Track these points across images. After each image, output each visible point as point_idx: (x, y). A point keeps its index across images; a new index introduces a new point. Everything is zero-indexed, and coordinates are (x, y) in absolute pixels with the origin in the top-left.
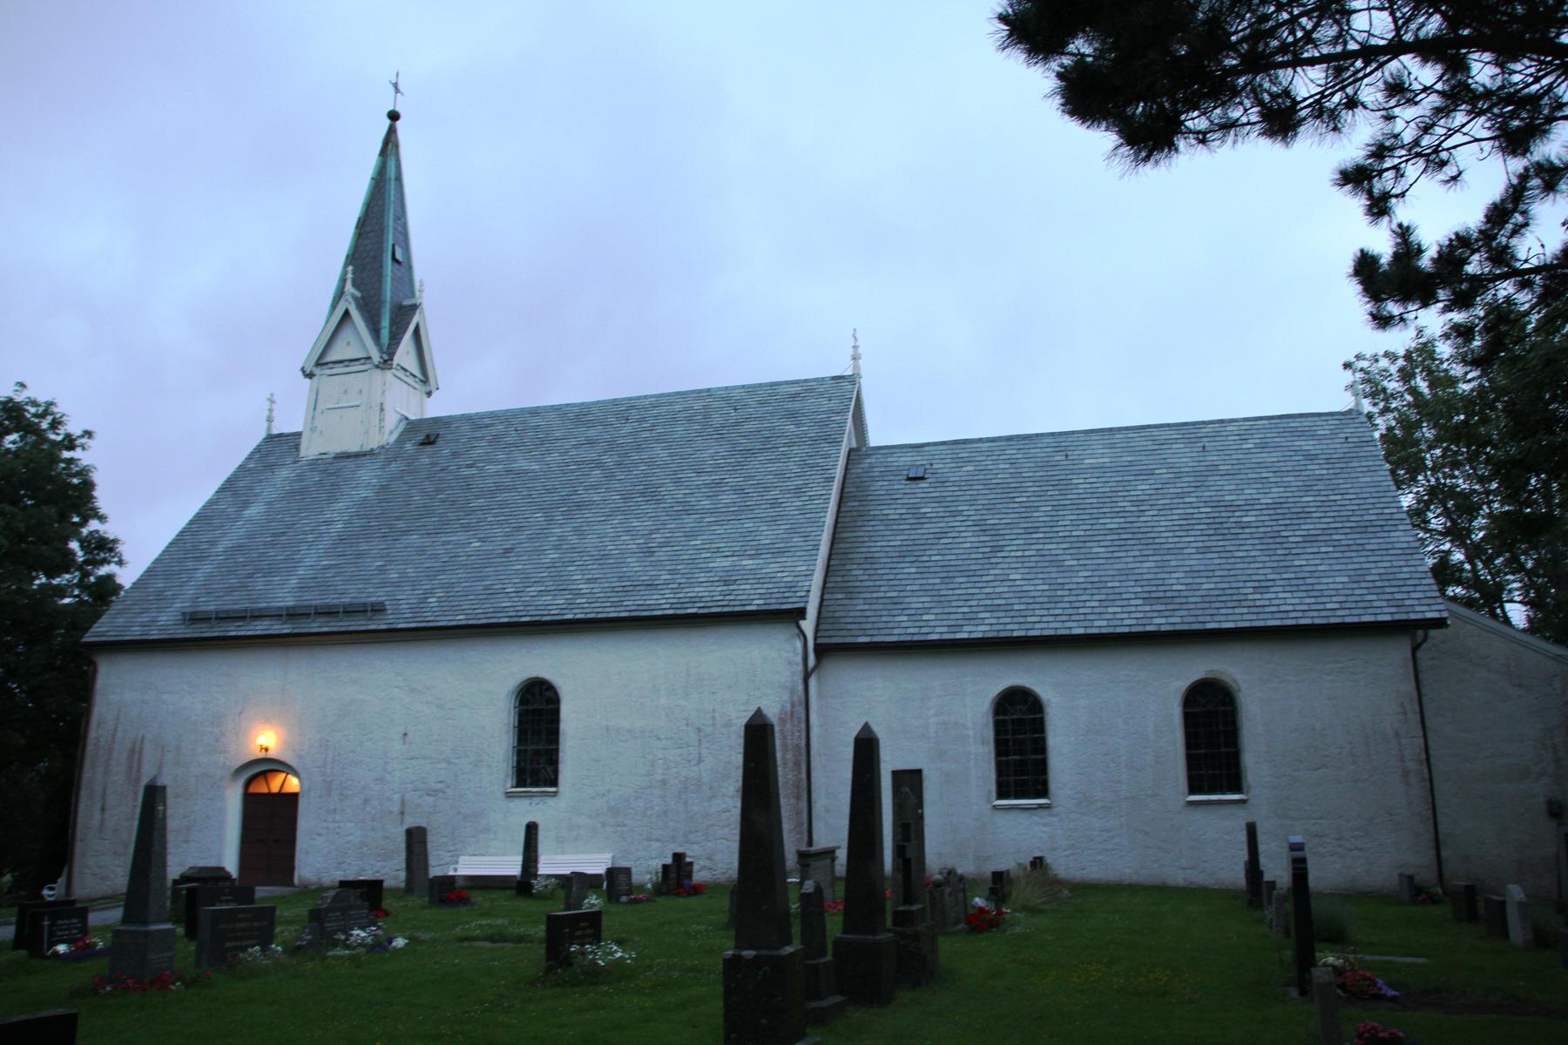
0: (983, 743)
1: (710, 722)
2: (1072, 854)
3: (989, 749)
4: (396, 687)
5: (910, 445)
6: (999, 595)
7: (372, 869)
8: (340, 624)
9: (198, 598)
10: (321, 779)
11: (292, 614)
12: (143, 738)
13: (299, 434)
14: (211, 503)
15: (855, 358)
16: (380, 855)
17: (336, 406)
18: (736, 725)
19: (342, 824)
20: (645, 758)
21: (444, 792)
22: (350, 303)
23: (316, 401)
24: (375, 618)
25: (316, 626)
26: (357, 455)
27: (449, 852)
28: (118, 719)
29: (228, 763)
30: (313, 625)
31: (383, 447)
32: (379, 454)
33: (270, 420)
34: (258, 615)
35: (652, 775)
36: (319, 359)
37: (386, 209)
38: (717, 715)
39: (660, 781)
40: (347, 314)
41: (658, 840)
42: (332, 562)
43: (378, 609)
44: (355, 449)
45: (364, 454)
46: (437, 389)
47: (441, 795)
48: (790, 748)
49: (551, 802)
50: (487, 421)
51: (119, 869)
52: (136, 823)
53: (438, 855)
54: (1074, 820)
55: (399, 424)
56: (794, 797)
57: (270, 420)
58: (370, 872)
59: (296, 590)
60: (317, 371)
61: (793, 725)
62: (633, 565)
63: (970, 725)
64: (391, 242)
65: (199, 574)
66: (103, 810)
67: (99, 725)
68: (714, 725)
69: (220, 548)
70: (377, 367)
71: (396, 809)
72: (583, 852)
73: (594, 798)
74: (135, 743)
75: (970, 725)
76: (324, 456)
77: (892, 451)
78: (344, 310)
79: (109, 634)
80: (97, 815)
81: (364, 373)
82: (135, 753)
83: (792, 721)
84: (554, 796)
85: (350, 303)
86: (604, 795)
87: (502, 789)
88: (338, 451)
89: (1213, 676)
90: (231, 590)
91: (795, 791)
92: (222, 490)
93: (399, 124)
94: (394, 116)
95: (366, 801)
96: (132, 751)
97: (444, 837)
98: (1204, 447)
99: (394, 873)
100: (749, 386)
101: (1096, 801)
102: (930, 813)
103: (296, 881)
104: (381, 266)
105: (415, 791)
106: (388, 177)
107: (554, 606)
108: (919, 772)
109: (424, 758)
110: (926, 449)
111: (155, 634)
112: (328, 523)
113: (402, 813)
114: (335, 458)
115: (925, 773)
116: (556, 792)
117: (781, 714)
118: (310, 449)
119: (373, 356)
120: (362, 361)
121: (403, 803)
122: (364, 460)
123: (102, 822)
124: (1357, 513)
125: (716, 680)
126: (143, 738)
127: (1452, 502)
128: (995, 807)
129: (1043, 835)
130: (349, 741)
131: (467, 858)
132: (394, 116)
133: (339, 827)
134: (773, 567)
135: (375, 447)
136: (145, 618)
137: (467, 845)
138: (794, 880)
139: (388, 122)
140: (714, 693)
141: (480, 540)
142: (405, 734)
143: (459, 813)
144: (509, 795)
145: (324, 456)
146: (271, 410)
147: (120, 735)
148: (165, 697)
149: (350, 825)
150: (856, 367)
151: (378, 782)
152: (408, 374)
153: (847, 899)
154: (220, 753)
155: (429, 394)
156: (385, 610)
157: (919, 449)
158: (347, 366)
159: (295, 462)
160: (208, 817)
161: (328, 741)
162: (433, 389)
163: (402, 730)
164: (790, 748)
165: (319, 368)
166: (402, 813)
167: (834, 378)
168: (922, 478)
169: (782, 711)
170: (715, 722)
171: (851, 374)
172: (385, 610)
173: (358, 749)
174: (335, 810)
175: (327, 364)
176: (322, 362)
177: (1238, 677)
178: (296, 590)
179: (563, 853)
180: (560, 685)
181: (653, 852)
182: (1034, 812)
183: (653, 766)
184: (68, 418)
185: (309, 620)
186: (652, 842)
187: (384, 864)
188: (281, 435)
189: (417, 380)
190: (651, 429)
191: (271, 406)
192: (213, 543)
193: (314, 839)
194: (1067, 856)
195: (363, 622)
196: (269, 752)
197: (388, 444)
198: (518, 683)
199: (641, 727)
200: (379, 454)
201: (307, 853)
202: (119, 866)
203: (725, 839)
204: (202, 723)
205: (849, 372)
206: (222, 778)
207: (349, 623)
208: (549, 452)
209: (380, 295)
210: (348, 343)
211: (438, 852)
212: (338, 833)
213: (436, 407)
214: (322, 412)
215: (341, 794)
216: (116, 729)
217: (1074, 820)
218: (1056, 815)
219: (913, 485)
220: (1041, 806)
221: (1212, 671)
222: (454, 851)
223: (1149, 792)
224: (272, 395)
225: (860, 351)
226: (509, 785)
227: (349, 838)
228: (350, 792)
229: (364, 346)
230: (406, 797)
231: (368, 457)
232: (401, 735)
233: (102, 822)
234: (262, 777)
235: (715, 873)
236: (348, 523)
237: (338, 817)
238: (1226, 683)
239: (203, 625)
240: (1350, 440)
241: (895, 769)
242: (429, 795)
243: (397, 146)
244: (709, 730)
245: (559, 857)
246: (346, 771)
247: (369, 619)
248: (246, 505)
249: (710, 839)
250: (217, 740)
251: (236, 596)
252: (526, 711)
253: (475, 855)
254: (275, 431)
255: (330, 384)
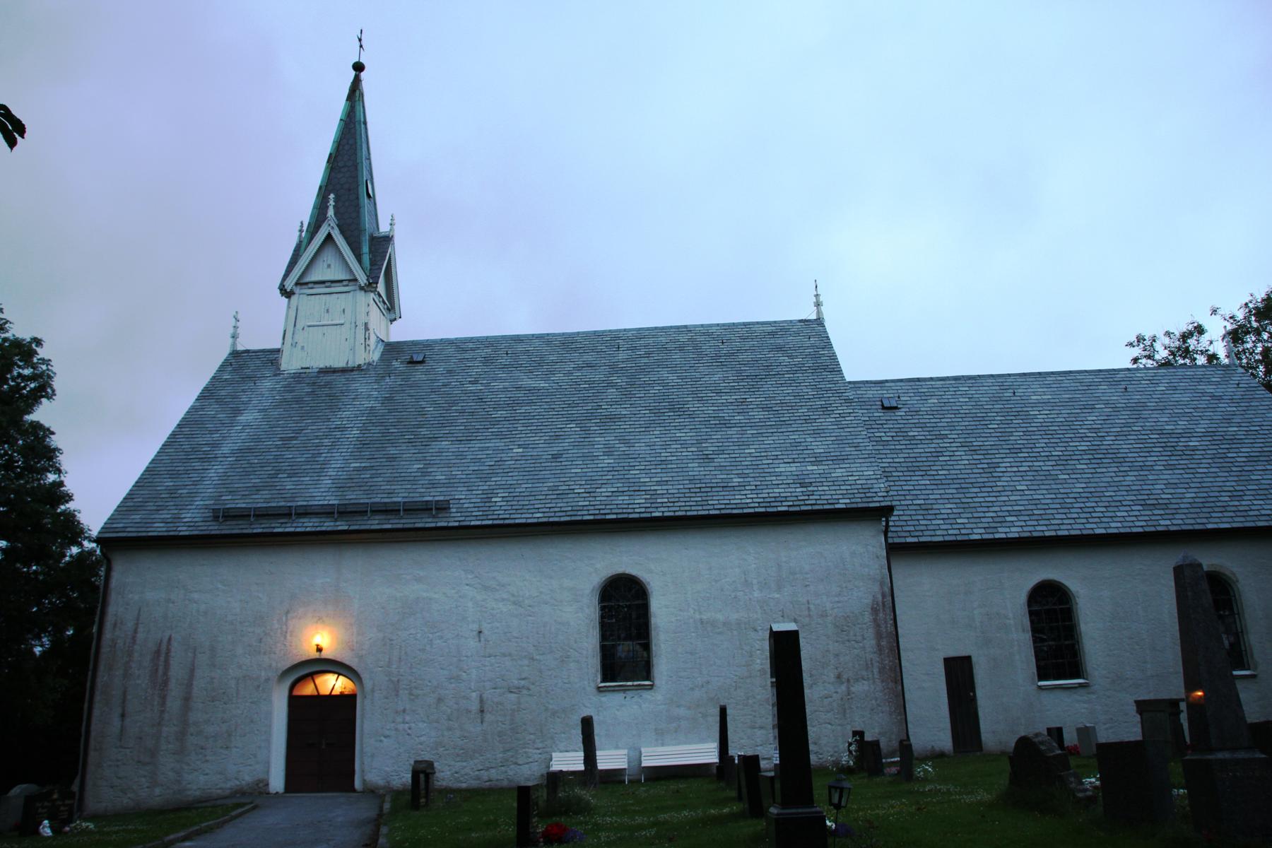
0: (1023, 631)
1: (807, 613)
2: (1111, 728)
3: (1028, 637)
4: (467, 585)
5: (871, 381)
6: (1016, 503)
7: (450, 770)
8: (402, 521)
9: (222, 496)
10: (387, 678)
11: (343, 512)
12: (170, 639)
13: (278, 351)
14: (193, 410)
15: (818, 305)
16: (458, 755)
17: (318, 323)
18: (831, 615)
19: (413, 725)
20: (742, 649)
21: (529, 689)
22: (333, 228)
23: (296, 316)
24: (440, 516)
25: (374, 523)
26: (344, 371)
27: (538, 749)
28: (138, 619)
29: (274, 664)
30: (369, 522)
31: (369, 364)
32: (368, 369)
33: (234, 337)
34: (306, 512)
35: (751, 665)
36: (299, 279)
37: (358, 147)
38: (812, 607)
39: (760, 671)
40: (329, 237)
41: (761, 728)
42: (363, 465)
43: (442, 507)
44: (340, 364)
45: (352, 370)
46: (400, 317)
47: (525, 692)
48: (884, 635)
49: (647, 695)
50: (471, 345)
51: (143, 780)
52: (769, 661)
53: (526, 752)
54: (1109, 697)
55: (377, 346)
56: (892, 681)
57: (234, 337)
58: (448, 773)
59: (333, 490)
60: (297, 290)
61: (886, 614)
62: (695, 468)
63: (1011, 615)
64: (365, 179)
65: (212, 473)
66: (123, 716)
67: (115, 625)
68: (809, 616)
69: (225, 450)
70: (362, 288)
71: (475, 707)
72: (685, 743)
73: (692, 689)
74: (160, 644)
75: (1011, 615)
76: (307, 371)
77: (857, 385)
78: (327, 233)
79: (129, 529)
80: (116, 722)
81: (347, 294)
82: (161, 654)
83: (884, 610)
84: (651, 689)
85: (333, 228)
86: (703, 686)
87: (593, 685)
88: (322, 366)
89: (1213, 569)
90: (257, 489)
91: (893, 675)
92: (201, 397)
93: (363, 75)
94: (359, 67)
95: (440, 700)
96: (158, 653)
97: (532, 734)
98: (1126, 389)
99: (477, 773)
100: (724, 325)
101: (1127, 679)
102: (982, 693)
103: (358, 784)
104: (358, 198)
105: (495, 688)
106: (357, 119)
107: (638, 506)
108: (968, 659)
109: (504, 655)
110: (887, 384)
111: (184, 530)
112: (342, 429)
113: (482, 711)
114: (319, 372)
115: (974, 660)
116: (652, 685)
117: (873, 604)
118: (291, 363)
119: (358, 277)
120: (345, 283)
121: (482, 701)
122: (355, 375)
123: (123, 729)
124: (987, 484)
125: (807, 573)
126: (170, 639)
127: (68, 633)
128: (1040, 687)
129: (1083, 711)
130: (416, 639)
131: (561, 754)
132: (359, 67)
133: (410, 729)
134: (839, 472)
135: (362, 362)
136: (165, 515)
137: (557, 742)
138: (896, 759)
139: (353, 73)
140: (806, 586)
141: (520, 446)
142: (480, 632)
143: (547, 709)
144: (600, 690)
145: (307, 371)
146: (817, 296)
147: (140, 636)
148: (196, 596)
149: (421, 725)
150: (819, 312)
151: (453, 680)
152: (381, 300)
153: (518, 807)
154: (265, 653)
155: (392, 321)
156: (449, 508)
157: (880, 385)
158: (312, 288)
159: (275, 375)
160: (252, 721)
161: (392, 640)
162: (398, 316)
163: (475, 627)
164: (884, 636)
165: (299, 287)
166: (482, 711)
167: (801, 321)
168: (896, 408)
169: (873, 601)
170: (811, 613)
171: (815, 318)
172: (449, 508)
173: (428, 648)
174: (404, 711)
175: (306, 284)
176: (302, 282)
177: (1235, 570)
178: (333, 490)
179: (663, 745)
180: (648, 580)
181: (758, 740)
182: (1073, 691)
183: (751, 657)
184: (11, 325)
185: (366, 518)
186: (756, 730)
187: (465, 764)
188: (247, 351)
189: (386, 307)
190: (648, 355)
191: (236, 324)
192: (215, 445)
193: (381, 741)
194: (1107, 729)
195: (430, 520)
196: (323, 652)
197: (373, 361)
198: (609, 575)
199: (737, 619)
200: (368, 369)
201: (373, 756)
202: (145, 776)
203: (829, 723)
204: (241, 623)
205: (814, 317)
206: (267, 680)
207: (413, 521)
208: (552, 373)
209: (358, 224)
210: (329, 266)
211: (527, 750)
212: (408, 734)
213: (400, 332)
214: (303, 329)
215: (411, 694)
216: (136, 631)
217: (1109, 697)
218: (1093, 693)
219: (890, 413)
220: (1081, 685)
221: (1212, 565)
222: (544, 748)
223: (1172, 670)
224: (237, 312)
225: (821, 299)
226: (599, 680)
227: (422, 739)
228: (420, 692)
229: (351, 271)
230: (485, 696)
231: (355, 373)
232: (475, 633)
233: (123, 729)
234: (310, 678)
235: (821, 756)
236: (364, 429)
237: (408, 718)
238: (1225, 575)
239: (240, 522)
240: (1240, 386)
241: (946, 657)
242: (511, 692)
243: (362, 95)
244: (807, 620)
245: (660, 749)
246: (414, 670)
247: (434, 517)
248: (237, 411)
249: (814, 724)
250: (260, 641)
251: (265, 494)
252: (604, 606)
253: (567, 751)
254: (240, 348)
255: (308, 303)
